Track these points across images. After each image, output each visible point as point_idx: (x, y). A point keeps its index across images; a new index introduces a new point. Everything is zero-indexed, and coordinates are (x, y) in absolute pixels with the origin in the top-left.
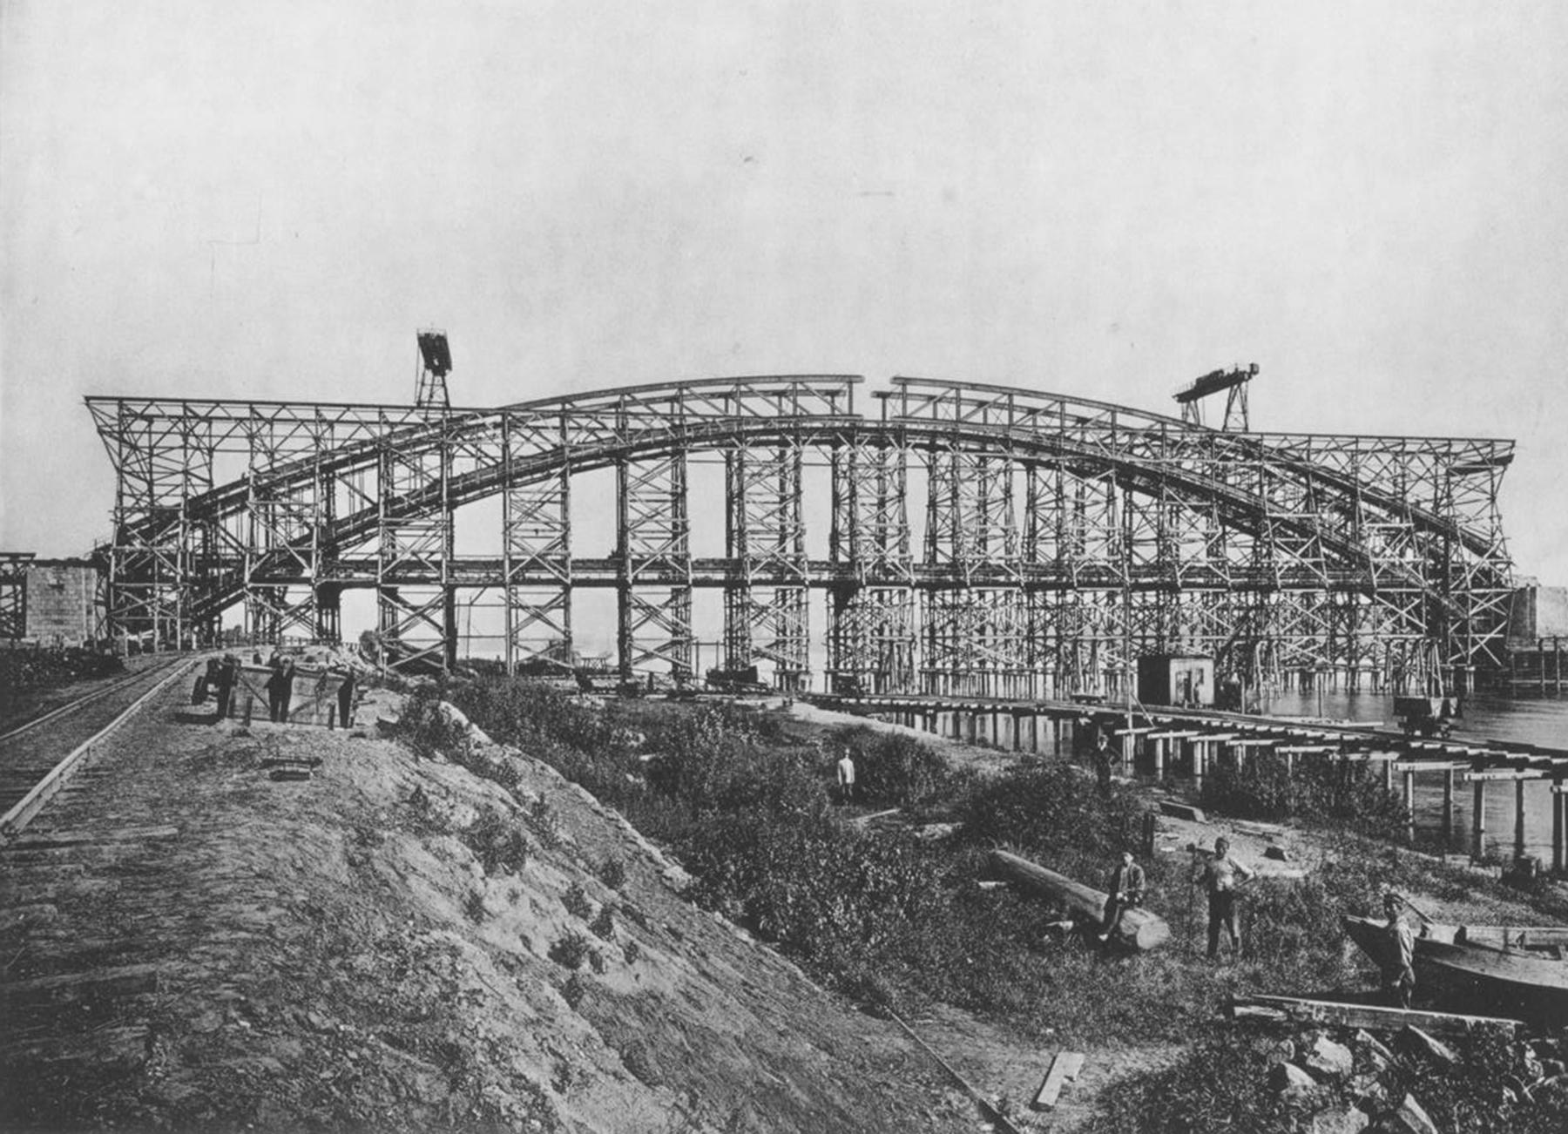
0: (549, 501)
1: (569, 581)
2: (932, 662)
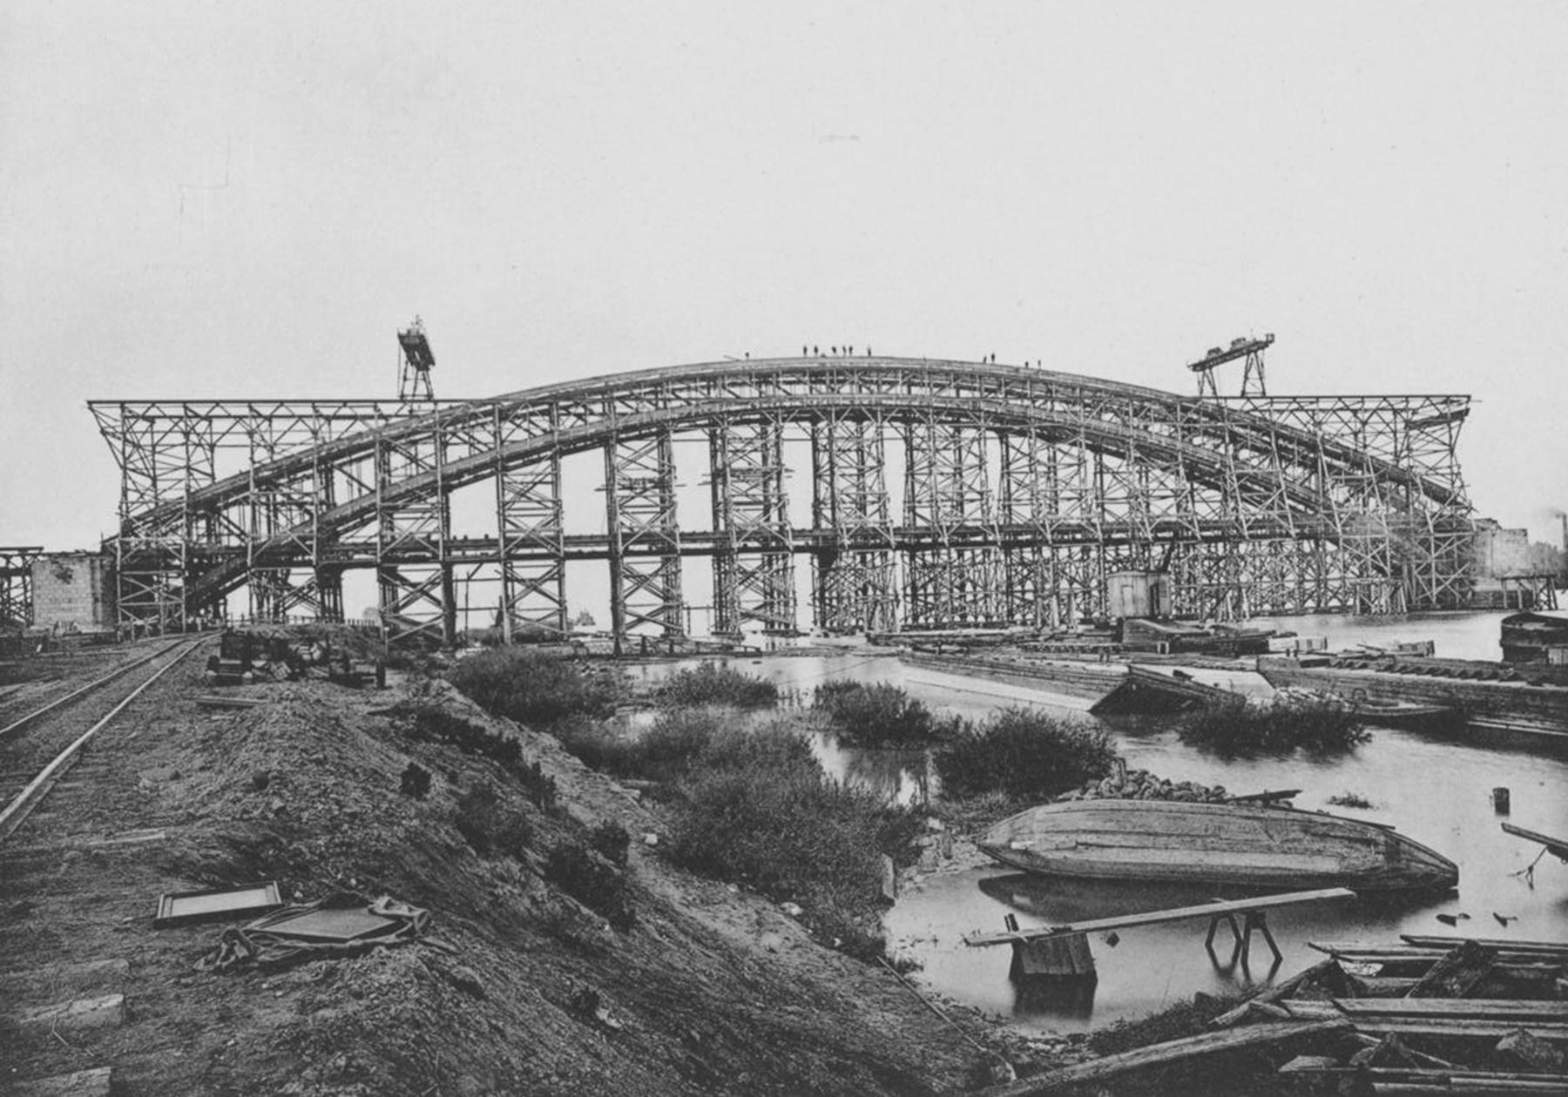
0: (540, 482)
1: (562, 555)
2: (916, 618)
